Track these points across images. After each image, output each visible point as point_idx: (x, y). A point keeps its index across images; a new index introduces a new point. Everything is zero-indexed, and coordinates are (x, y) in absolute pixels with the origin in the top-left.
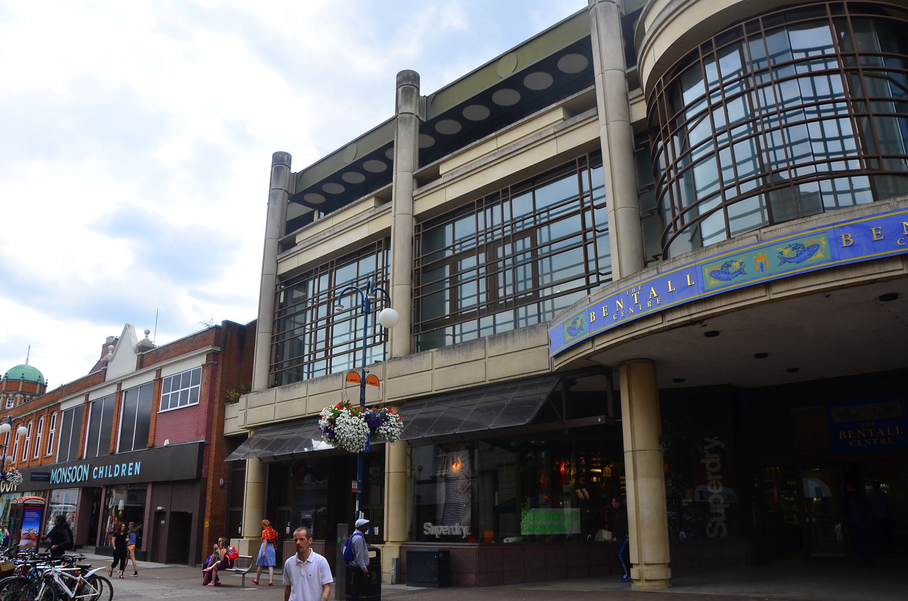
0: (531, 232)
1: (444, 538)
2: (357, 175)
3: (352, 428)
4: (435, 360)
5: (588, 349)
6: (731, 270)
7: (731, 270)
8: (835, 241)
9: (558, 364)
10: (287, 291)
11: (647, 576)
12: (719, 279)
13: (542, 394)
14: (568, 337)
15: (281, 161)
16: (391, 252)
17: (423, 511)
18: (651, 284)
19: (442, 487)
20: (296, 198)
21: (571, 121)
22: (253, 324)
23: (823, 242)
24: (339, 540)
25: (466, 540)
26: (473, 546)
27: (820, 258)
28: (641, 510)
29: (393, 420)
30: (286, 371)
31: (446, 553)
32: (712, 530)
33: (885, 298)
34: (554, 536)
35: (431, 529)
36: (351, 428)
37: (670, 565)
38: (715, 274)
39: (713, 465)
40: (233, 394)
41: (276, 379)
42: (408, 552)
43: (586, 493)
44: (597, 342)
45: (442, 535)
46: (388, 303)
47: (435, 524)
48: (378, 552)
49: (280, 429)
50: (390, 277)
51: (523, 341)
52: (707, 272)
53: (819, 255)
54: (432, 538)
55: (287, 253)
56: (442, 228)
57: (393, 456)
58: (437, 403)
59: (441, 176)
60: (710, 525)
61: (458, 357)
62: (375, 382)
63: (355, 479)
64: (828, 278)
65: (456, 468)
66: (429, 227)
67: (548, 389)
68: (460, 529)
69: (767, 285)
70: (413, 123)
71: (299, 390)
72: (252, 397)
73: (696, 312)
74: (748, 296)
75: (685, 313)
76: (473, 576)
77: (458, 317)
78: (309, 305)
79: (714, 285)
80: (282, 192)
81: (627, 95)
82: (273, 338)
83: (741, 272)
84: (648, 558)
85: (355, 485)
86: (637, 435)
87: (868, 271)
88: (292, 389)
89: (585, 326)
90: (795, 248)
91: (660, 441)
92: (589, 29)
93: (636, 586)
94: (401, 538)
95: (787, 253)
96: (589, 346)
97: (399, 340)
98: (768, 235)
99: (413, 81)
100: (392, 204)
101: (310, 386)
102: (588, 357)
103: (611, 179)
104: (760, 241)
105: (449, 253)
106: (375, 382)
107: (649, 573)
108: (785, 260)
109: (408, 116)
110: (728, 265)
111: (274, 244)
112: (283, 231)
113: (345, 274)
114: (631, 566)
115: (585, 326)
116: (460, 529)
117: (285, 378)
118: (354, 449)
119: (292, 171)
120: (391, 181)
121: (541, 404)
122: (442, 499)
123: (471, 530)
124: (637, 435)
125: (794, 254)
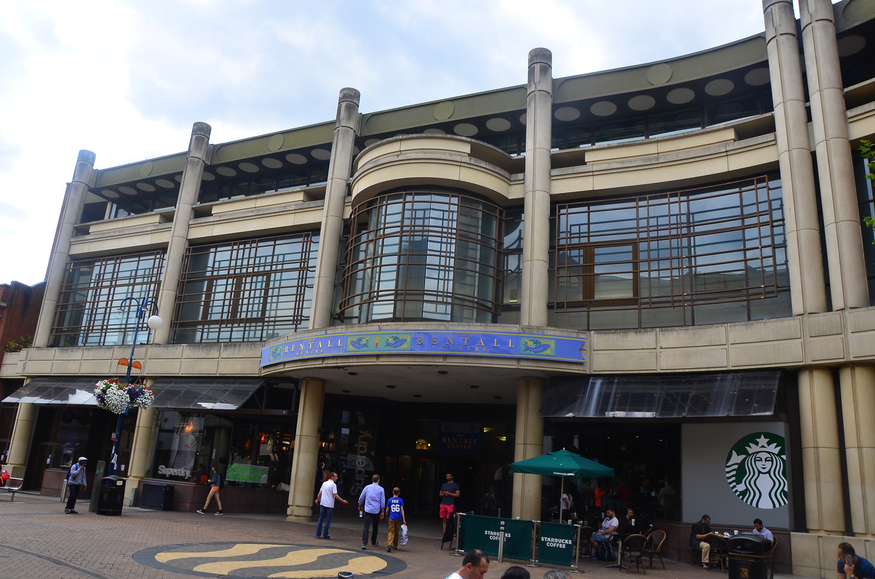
0: (268, 274)
1: (172, 477)
2: (146, 191)
3: (118, 397)
4: (185, 352)
5: (280, 369)
6: (362, 343)
7: (362, 343)
8: (414, 339)
9: (264, 373)
10: (76, 271)
11: (296, 513)
12: (354, 346)
13: (253, 388)
14: (272, 358)
15: (85, 159)
16: (166, 256)
17: (161, 455)
18: (320, 339)
19: (176, 437)
20: (96, 191)
21: (307, 204)
22: (40, 289)
23: (409, 339)
24: (97, 471)
25: (188, 480)
26: (191, 484)
27: (405, 348)
28: (299, 472)
29: (147, 395)
30: (66, 335)
31: (172, 488)
32: (354, 491)
33: (441, 372)
34: (246, 483)
35: (163, 470)
36: (117, 397)
37: (312, 508)
38: (353, 343)
39: (362, 449)
40: (13, 344)
41: (55, 340)
42: (145, 485)
43: (277, 457)
44: (287, 366)
45: (171, 475)
46: (155, 311)
47: (167, 467)
48: (124, 482)
49: (58, 381)
50: (162, 278)
51: (245, 351)
52: (349, 340)
53: (405, 346)
54: (163, 476)
55: (80, 238)
56: (208, 248)
57: (143, 419)
58: (181, 383)
59: (212, 215)
60: (353, 488)
61: (201, 353)
62: (138, 366)
63: (115, 432)
64: (407, 359)
65: (189, 428)
66: (198, 250)
67: (257, 386)
68: (184, 472)
69: (378, 356)
70: (199, 167)
71: (76, 354)
72: (32, 352)
73: (340, 363)
74: (367, 360)
75: (334, 361)
76: (188, 505)
77: (206, 322)
78: (92, 285)
79: (351, 350)
80: (83, 185)
81: (344, 198)
82: (57, 306)
83: (366, 345)
84: (298, 503)
85: (114, 436)
86: (305, 425)
87: (427, 359)
88: (69, 352)
89: (282, 354)
90: (395, 338)
91: (319, 431)
92: (333, 138)
93: (289, 519)
94: (141, 474)
95: (391, 340)
96: (282, 367)
97: (161, 334)
98: (385, 327)
99: (205, 132)
100: (172, 225)
101: (86, 352)
102: (282, 373)
103: (323, 251)
104: (380, 330)
105: (208, 274)
106: (138, 366)
107: (297, 511)
108: (388, 344)
109: (196, 160)
110: (360, 340)
111: (68, 228)
112: (79, 219)
113: (127, 266)
114: (288, 506)
115: (282, 354)
116: (184, 472)
117: (62, 342)
118: (118, 411)
119: (95, 168)
120: (174, 204)
121: (251, 393)
122: (175, 447)
123: (192, 474)
124: (305, 425)
125: (393, 342)
